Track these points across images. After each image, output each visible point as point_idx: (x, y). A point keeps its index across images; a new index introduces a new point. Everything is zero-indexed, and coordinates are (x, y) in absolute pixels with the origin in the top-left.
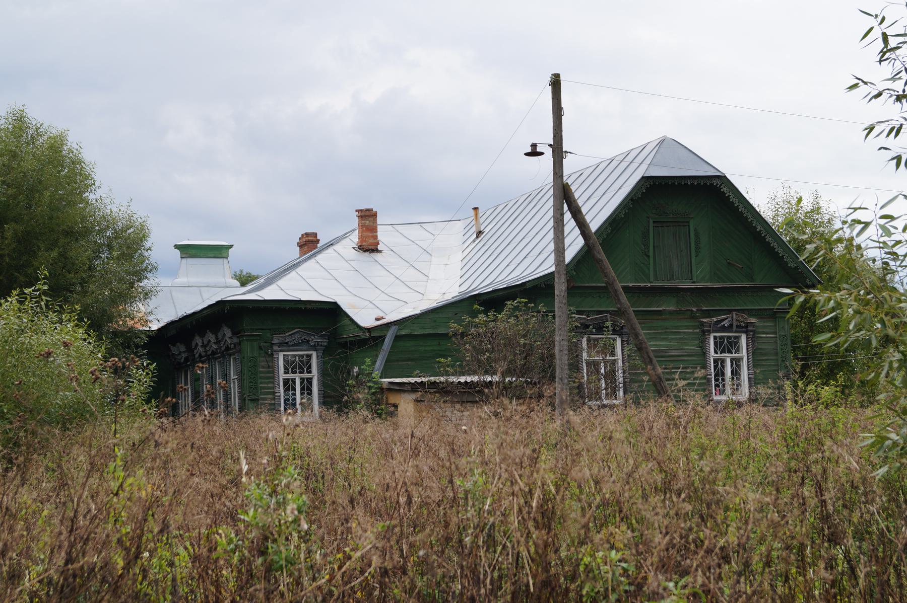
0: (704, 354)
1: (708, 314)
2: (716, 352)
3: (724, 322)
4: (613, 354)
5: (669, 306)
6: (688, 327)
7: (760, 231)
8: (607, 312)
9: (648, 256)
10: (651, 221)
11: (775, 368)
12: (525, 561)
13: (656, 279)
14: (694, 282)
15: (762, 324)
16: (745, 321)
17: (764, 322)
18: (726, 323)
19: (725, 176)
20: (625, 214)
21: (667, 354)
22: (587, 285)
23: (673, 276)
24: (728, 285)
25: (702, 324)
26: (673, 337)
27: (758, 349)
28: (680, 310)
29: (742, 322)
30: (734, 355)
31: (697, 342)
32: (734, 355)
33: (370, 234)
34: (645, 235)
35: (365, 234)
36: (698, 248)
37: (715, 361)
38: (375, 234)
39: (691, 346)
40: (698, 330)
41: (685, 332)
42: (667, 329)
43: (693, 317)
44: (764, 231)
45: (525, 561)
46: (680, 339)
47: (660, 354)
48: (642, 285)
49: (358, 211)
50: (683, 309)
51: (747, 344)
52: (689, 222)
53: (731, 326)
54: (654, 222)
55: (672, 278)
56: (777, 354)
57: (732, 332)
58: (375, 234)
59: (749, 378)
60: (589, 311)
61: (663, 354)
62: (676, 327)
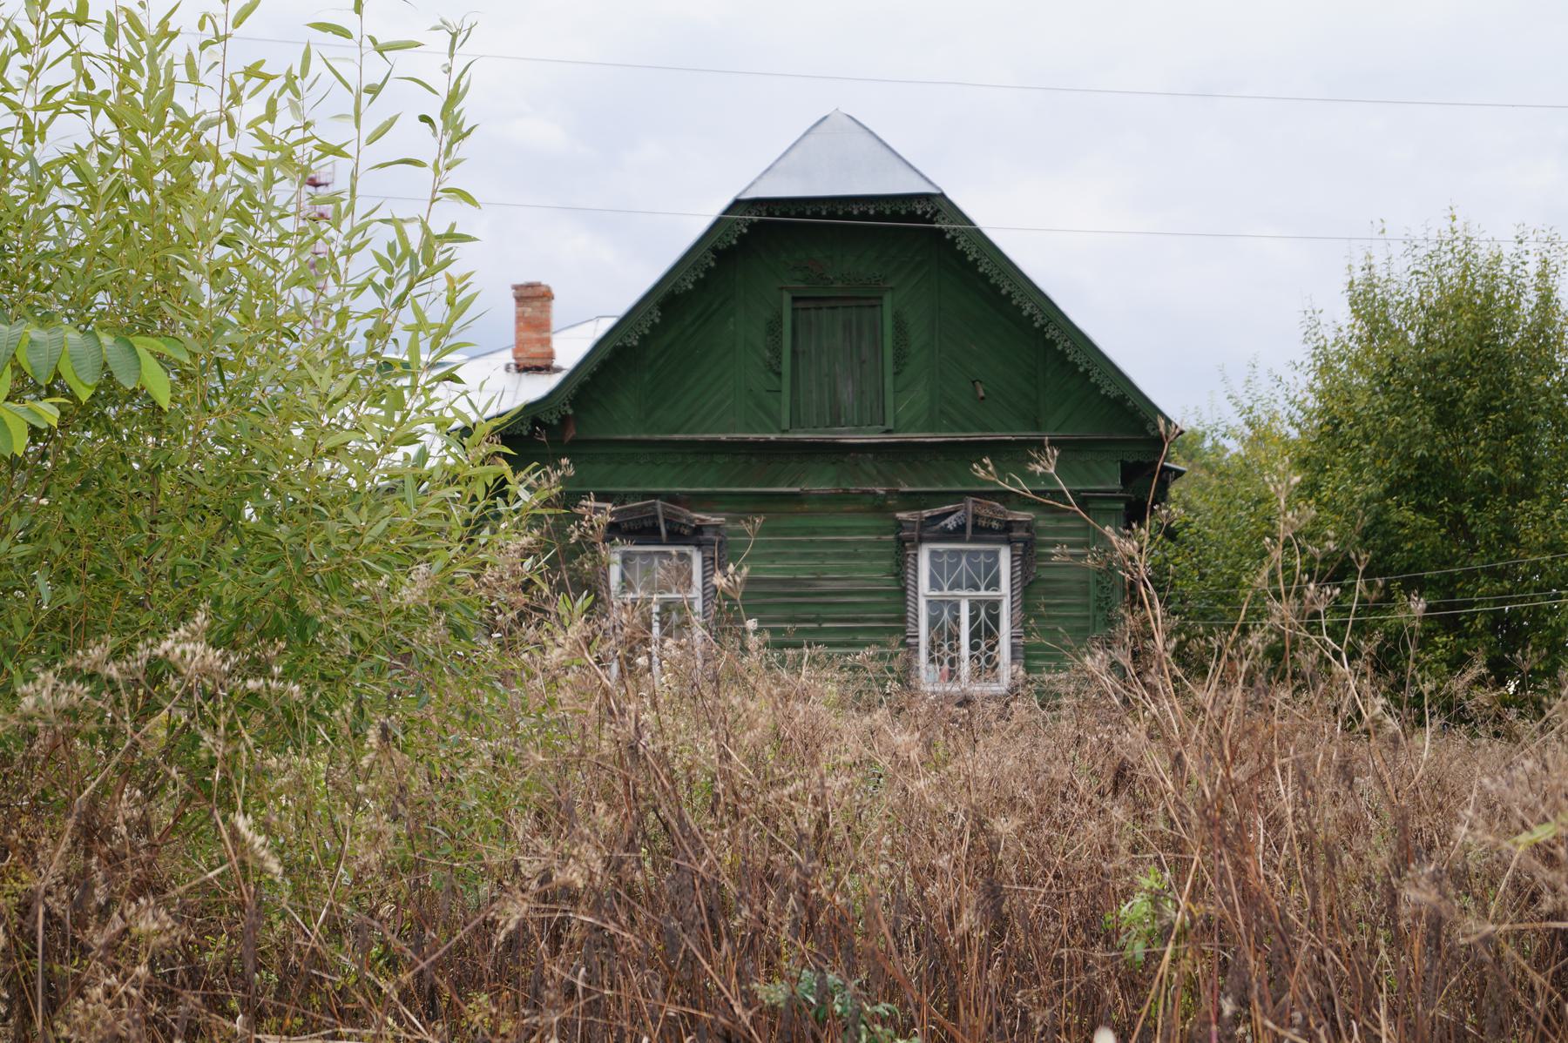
0: (902, 591)
1: (913, 501)
2: (935, 584)
3: (947, 521)
4: (994, 583)
5: (819, 484)
6: (865, 531)
7: (1031, 316)
8: (655, 495)
9: (779, 374)
10: (787, 297)
11: (1079, 624)
12: (40, 1014)
13: (796, 423)
14: (888, 431)
15: (1052, 524)
16: (1000, 517)
17: (1059, 520)
18: (951, 523)
19: (942, 195)
20: (697, 283)
21: (812, 589)
22: (629, 437)
23: (839, 418)
24: (961, 437)
25: (900, 525)
26: (829, 551)
27: (1038, 580)
28: (847, 492)
29: (992, 519)
30: (983, 593)
31: (887, 563)
32: (983, 593)
33: (534, 335)
34: (774, 327)
35: (525, 335)
36: (900, 358)
37: (933, 604)
38: (545, 335)
39: (873, 573)
40: (891, 537)
41: (860, 542)
42: (814, 533)
43: (880, 507)
44: (1039, 316)
45: (40, 1014)
46: (846, 556)
47: (794, 590)
48: (752, 436)
49: (516, 288)
50: (852, 489)
51: (1012, 568)
52: (881, 298)
53: (961, 529)
54: (795, 299)
55: (836, 421)
56: (1087, 593)
57: (963, 541)
58: (545, 335)
59: (1013, 646)
60: (626, 495)
61: (804, 589)
62: (838, 530)
